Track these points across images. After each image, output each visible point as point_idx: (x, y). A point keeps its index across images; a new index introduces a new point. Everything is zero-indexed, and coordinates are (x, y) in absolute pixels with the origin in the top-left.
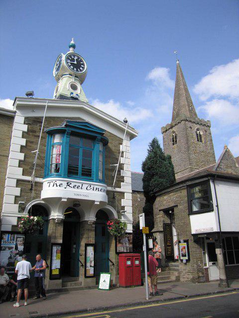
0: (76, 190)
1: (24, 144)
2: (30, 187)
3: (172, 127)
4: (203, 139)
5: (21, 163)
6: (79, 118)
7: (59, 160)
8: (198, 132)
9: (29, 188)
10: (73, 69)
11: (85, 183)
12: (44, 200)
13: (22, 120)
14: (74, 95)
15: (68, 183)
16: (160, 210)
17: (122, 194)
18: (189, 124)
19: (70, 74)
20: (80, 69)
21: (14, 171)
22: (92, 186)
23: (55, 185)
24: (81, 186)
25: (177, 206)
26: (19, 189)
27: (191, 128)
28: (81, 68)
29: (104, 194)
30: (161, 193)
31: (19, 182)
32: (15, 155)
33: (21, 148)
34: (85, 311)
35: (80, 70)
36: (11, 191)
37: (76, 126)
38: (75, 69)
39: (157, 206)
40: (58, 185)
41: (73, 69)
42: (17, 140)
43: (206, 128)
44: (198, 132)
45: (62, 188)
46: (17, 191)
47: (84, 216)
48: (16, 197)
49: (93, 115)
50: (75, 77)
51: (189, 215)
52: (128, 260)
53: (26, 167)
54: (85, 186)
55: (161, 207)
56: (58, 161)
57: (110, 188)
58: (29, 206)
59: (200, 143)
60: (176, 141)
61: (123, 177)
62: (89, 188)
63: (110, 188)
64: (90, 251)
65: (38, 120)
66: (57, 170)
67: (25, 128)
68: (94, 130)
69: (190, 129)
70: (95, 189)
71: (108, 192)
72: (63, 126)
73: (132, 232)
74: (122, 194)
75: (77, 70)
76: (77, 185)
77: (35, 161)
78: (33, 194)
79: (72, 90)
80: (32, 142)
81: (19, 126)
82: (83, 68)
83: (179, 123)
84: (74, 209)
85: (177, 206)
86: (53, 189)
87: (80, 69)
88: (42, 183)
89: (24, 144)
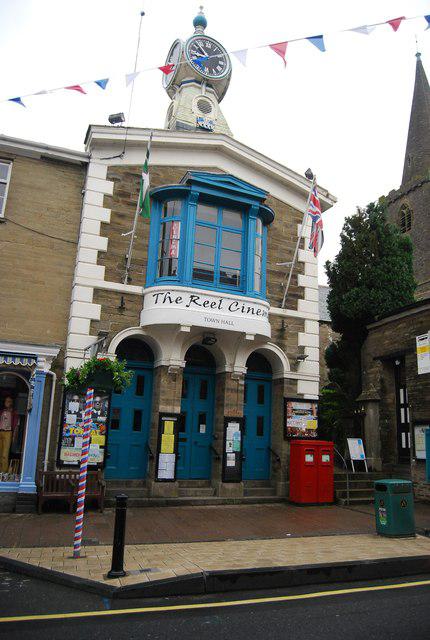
0: (208, 310)
1: (107, 219)
9: (122, 307)
12: (145, 328)
13: (104, 173)
14: (205, 124)
15: (192, 297)
16: (374, 359)
19: (196, 81)
21: (90, 274)
22: (240, 305)
26: (98, 307)
28: (219, 68)
29: (265, 319)
31: (99, 294)
32: (92, 242)
33: (101, 227)
35: (217, 71)
40: (173, 299)
42: (95, 212)
45: (181, 306)
46: (96, 312)
48: (92, 321)
50: (208, 85)
52: (310, 452)
54: (226, 304)
60: (410, 224)
62: (233, 308)
65: (132, 174)
67: (109, 188)
70: (246, 310)
71: (272, 317)
75: (211, 72)
79: (196, 109)
80: (121, 216)
81: (99, 185)
84: (205, 348)
86: (174, 308)
89: (107, 219)
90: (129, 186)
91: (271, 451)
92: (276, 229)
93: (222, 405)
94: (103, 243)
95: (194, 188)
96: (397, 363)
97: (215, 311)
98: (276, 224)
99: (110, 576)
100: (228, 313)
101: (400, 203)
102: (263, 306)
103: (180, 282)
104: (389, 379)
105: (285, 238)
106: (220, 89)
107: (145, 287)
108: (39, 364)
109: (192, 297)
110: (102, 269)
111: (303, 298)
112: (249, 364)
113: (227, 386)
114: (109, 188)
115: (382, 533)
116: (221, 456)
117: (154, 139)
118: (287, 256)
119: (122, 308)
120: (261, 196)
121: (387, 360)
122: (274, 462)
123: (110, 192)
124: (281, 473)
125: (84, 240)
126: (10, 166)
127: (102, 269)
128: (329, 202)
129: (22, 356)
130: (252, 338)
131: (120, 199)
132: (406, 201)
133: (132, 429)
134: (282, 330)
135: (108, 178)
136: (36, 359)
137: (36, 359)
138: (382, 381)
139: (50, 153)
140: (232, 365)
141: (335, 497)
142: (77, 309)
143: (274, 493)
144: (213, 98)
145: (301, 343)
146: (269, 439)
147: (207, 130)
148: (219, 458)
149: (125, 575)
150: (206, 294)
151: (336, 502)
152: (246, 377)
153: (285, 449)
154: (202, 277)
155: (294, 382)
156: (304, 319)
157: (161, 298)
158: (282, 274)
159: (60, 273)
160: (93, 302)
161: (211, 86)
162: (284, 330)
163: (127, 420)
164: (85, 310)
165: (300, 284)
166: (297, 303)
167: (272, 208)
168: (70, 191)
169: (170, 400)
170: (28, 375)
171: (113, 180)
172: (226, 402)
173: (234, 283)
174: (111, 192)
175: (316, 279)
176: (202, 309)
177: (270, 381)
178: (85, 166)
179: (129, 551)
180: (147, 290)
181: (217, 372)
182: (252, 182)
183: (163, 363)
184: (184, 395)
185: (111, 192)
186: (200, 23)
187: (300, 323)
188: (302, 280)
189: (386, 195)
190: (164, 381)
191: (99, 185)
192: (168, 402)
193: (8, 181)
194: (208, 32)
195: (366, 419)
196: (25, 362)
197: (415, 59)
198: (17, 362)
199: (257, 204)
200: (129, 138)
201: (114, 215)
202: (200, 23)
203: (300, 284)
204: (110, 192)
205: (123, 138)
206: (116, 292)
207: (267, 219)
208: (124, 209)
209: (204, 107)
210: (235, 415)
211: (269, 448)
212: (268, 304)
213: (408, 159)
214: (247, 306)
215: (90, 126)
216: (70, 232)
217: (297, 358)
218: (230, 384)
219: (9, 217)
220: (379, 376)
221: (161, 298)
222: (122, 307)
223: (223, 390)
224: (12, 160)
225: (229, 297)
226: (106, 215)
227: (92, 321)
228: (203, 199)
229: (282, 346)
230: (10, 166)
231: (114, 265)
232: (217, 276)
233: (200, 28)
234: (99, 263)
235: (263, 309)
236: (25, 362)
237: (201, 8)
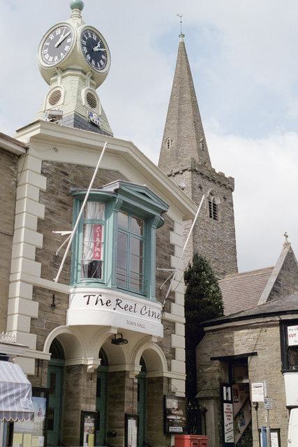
1: (42, 216)
4: (219, 214)
10: (91, 61)
12: (71, 327)
14: (94, 118)
15: (117, 300)
16: (213, 359)
19: (82, 71)
21: (24, 266)
22: (147, 310)
23: (99, 302)
24: (134, 306)
25: (254, 354)
26: (36, 304)
27: (201, 188)
28: (101, 61)
29: (159, 322)
31: (38, 292)
32: (26, 239)
36: (21, 307)
38: (93, 62)
40: (104, 302)
43: (226, 192)
44: (212, 198)
45: (110, 309)
48: (32, 319)
49: (93, 149)
51: (283, 372)
53: (47, 263)
55: (215, 353)
56: (97, 255)
59: (213, 221)
62: (143, 312)
64: (132, 424)
67: (42, 183)
69: (198, 190)
70: (151, 314)
73: (184, 396)
75: (96, 65)
80: (52, 212)
82: (104, 61)
83: (177, 173)
85: (254, 354)
86: (86, 309)
87: (100, 64)
88: (66, 298)
89: (42, 216)
94: (38, 240)
106: (97, 80)
110: (39, 265)
127: (39, 265)
142: (15, 306)
147: (94, 126)
155: (169, 380)
157: (93, 300)
160: (33, 300)
175: (179, 276)
184: (98, 395)
189: (227, 176)
190: (83, 381)
191: (32, 182)
192: (87, 400)
195: (207, 414)
201: (49, 212)
204: (44, 188)
217: (172, 354)
218: (128, 383)
220: (217, 376)
221: (93, 300)
222: (53, 303)
227: (32, 319)
231: (47, 263)
234: (37, 260)
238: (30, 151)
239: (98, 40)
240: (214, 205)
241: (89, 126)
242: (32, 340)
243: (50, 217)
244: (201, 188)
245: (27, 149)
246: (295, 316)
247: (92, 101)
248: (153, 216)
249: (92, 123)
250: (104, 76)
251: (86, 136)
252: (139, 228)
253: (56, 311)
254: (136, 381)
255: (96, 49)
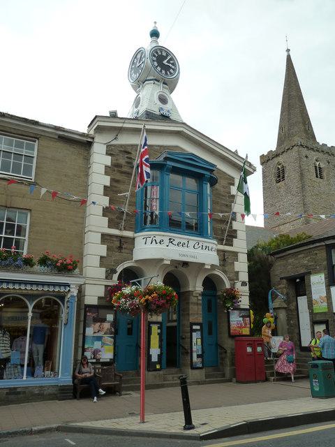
0: (180, 248)
1: (108, 184)
2: (117, 244)
3: (277, 155)
4: (324, 174)
5: (106, 212)
6: (177, 147)
7: (156, 206)
8: (318, 163)
9: (120, 246)
10: (161, 71)
11: (193, 240)
12: (136, 261)
13: (103, 149)
14: (165, 112)
15: (170, 239)
16: (282, 279)
17: (235, 254)
18: (305, 152)
20: (170, 72)
21: (96, 223)
22: (200, 245)
23: (154, 242)
24: (186, 244)
27: (307, 157)
28: (171, 71)
29: (215, 253)
30: (284, 254)
31: (105, 238)
32: (98, 200)
33: (104, 189)
34: (31, 433)
35: (171, 73)
37: (179, 159)
38: (164, 72)
39: (277, 273)
41: (161, 71)
42: (99, 179)
43: (329, 158)
44: (318, 163)
45: (163, 246)
46: (103, 250)
47: (187, 284)
48: (101, 257)
50: (164, 83)
52: (249, 345)
54: (191, 244)
57: (221, 247)
58: (120, 269)
59: (319, 180)
60: (283, 177)
61: (236, 231)
63: (221, 247)
65: (127, 151)
66: (152, 222)
67: (108, 160)
68: (200, 165)
70: (204, 248)
71: (219, 251)
72: (162, 159)
74: (235, 255)
75: (166, 74)
76: (182, 241)
77: (126, 209)
78: (125, 253)
79: (159, 103)
80: (117, 181)
81: (100, 159)
82: (173, 69)
84: (175, 275)
86: (153, 247)
87: (170, 72)
88: (132, 241)
89: (108, 184)
90: (122, 161)
91: (219, 346)
92: (217, 189)
93: (188, 314)
94: (105, 201)
95: (168, 163)
96: (298, 280)
97: (185, 249)
98: (217, 186)
99: (185, 428)
100: (193, 250)
101: (276, 160)
102: (213, 244)
103: (159, 229)
104: (292, 292)
105: (223, 196)
106: (171, 85)
107: (136, 233)
108: (72, 290)
109: (170, 239)
110: (106, 219)
111: (236, 237)
112: (204, 284)
113: (191, 301)
114: (108, 160)
115: (315, 395)
116: (189, 351)
117: (147, 127)
118: (226, 209)
119: (120, 248)
120: (211, 168)
121: (291, 280)
122: (221, 354)
123: (109, 164)
124: (228, 362)
125: (91, 199)
126: (36, 144)
127: (106, 219)
128: (251, 170)
129: (60, 285)
130: (209, 267)
131: (116, 169)
132: (280, 159)
133: (127, 331)
134: (224, 260)
135: (107, 154)
136: (69, 286)
137: (69, 286)
138: (287, 294)
139: (66, 134)
140: (195, 287)
141: (266, 377)
143: (224, 375)
144: (167, 91)
145: (236, 270)
146: (217, 337)
148: (187, 353)
149: (193, 428)
150: (179, 237)
151: (267, 380)
152: (203, 294)
153: (229, 344)
154: (174, 225)
156: (238, 253)
157: (149, 240)
158: (223, 221)
159: (75, 223)
161: (166, 84)
162: (226, 259)
163: (123, 328)
164: (94, 250)
165: (234, 228)
166: (232, 242)
167: (215, 175)
168: (81, 161)
169: (196, 313)
170: (62, 298)
171: (110, 155)
172: (191, 312)
173: (196, 229)
174: (109, 164)
176: (176, 248)
177: (215, 296)
178: (89, 144)
179: (194, 414)
180: (136, 235)
181: (182, 291)
182: (201, 157)
183: (191, 289)
185: (109, 164)
186: (155, 34)
187: (235, 255)
188: (235, 225)
191: (100, 159)
193: (35, 155)
194: (162, 42)
196: (62, 289)
197: (286, 54)
198: (57, 289)
199: (209, 174)
200: (125, 125)
201: (112, 180)
202: (155, 34)
203: (234, 228)
204: (109, 164)
205: (120, 125)
206: (117, 236)
207: (213, 182)
208: (118, 177)
209: (163, 100)
210: (197, 321)
211: (217, 343)
212: (216, 243)
213: (281, 128)
214: (205, 245)
215: (96, 117)
216: (152, 213)
218: (193, 300)
219: (38, 182)
221: (149, 240)
222: (120, 246)
223: (188, 303)
224: (38, 139)
225: (193, 239)
226: (107, 181)
227: (101, 257)
228: (175, 171)
229: (225, 272)
230: (36, 144)
232: (184, 224)
233: (154, 38)
235: (214, 246)
236: (62, 289)
237: (155, 23)
238: (96, 140)
239: (167, 55)
240: (320, 168)
241: (161, 117)
242: (102, 272)
243: (115, 184)
244: (307, 157)
245: (93, 138)
246: (332, 241)
247: (163, 100)
248: (203, 175)
249: (162, 115)
250: (177, 80)
251: (165, 124)
252: (194, 180)
253: (123, 251)
254: (200, 298)
255: (165, 62)
